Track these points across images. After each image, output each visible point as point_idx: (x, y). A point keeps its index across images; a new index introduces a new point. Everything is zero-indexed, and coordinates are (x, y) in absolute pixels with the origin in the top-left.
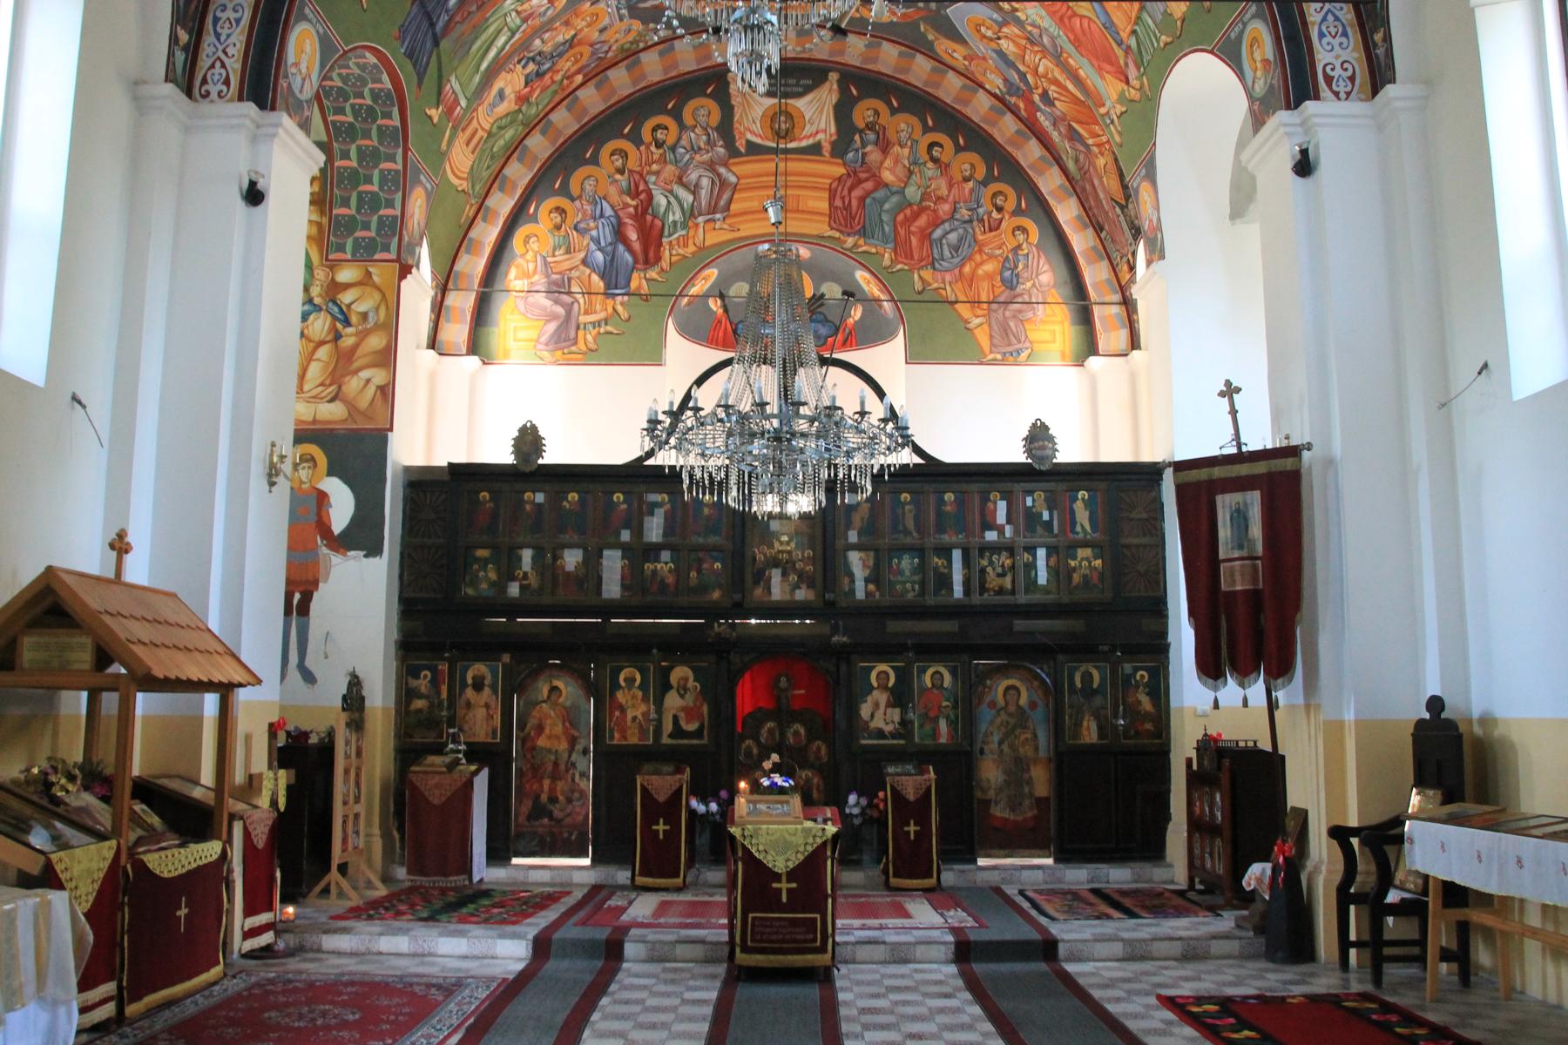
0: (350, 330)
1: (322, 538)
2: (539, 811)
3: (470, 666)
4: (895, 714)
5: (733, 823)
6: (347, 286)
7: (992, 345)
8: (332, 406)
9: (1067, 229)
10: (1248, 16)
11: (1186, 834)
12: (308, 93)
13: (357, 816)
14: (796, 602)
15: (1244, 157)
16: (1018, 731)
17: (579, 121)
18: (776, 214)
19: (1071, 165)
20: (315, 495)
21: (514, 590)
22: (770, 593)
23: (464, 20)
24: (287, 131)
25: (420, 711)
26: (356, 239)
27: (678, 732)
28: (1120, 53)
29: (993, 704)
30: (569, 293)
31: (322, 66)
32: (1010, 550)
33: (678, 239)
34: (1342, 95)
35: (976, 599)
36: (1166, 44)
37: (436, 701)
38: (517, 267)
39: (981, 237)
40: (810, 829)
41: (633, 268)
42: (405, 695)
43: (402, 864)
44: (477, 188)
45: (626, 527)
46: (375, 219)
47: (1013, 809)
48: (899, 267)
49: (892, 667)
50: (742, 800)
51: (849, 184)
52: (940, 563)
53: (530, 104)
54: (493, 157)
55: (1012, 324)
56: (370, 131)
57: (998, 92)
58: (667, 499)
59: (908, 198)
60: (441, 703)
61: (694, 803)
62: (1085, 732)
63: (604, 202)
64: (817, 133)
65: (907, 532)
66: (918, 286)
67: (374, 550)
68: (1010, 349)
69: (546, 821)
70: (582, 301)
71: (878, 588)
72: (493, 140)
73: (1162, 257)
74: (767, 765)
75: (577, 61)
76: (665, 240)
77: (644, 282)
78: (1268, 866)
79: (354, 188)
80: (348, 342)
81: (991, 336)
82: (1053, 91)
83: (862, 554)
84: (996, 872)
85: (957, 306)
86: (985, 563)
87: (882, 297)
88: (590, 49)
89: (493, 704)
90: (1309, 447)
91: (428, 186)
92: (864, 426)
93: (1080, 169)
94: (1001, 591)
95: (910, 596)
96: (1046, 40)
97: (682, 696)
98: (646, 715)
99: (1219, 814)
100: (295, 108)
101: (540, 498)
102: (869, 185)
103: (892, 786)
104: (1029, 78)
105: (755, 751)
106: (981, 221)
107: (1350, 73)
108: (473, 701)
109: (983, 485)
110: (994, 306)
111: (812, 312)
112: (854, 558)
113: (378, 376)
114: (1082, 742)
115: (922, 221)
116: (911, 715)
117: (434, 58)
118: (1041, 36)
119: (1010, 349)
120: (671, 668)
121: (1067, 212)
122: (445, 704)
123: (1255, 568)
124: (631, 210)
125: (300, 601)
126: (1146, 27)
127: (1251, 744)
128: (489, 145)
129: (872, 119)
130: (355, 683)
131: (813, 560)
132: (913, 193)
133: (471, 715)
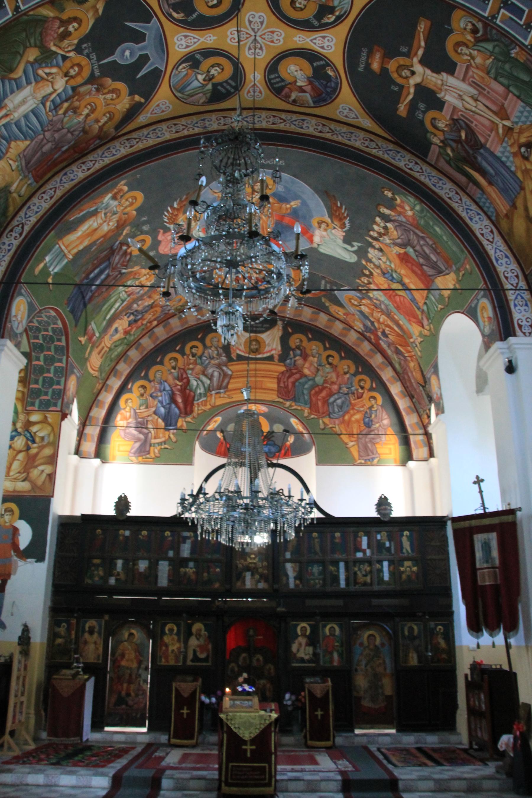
0: (35, 445)
1: (15, 552)
2: (121, 701)
4: (310, 650)
5: (221, 712)
8: (23, 484)
9: (396, 398)
12: (20, 329)
13: (22, 703)
17: (154, 343)
18: (247, 394)
19: (397, 366)
21: (112, 581)
23: (99, 295)
25: (59, 645)
27: (196, 658)
28: (419, 313)
29: (361, 644)
30: (147, 428)
31: (29, 317)
32: (369, 562)
33: (202, 402)
34: (527, 334)
35: (352, 588)
36: (441, 309)
38: (121, 414)
39: (353, 402)
41: (179, 416)
42: (52, 635)
43: (45, 730)
44: (103, 375)
46: (50, 391)
48: (312, 416)
49: (309, 625)
50: (227, 699)
51: (287, 375)
55: (369, 445)
57: (360, 330)
61: (203, 698)
62: (411, 659)
63: (166, 384)
64: (272, 350)
65: (316, 553)
66: (322, 426)
67: (40, 558)
68: (369, 458)
69: (124, 706)
70: (153, 432)
73: (443, 412)
74: (241, 679)
75: (154, 315)
76: (195, 402)
77: (184, 423)
79: (41, 375)
80: (33, 451)
81: (359, 451)
83: (293, 565)
84: (365, 738)
85: (342, 436)
86: (356, 569)
87: (304, 432)
89: (98, 642)
90: (520, 509)
91: (78, 374)
93: (402, 368)
94: (365, 584)
95: (318, 586)
97: (198, 639)
98: (179, 649)
100: (14, 337)
101: (127, 533)
102: (297, 376)
104: (376, 324)
106: (353, 393)
108: (88, 640)
109: (355, 528)
110: (360, 436)
112: (289, 566)
113: (48, 469)
114: (409, 665)
115: (324, 394)
116: (318, 651)
117: (84, 313)
118: (380, 305)
119: (369, 458)
121: (396, 389)
122: (74, 641)
124: (179, 387)
126: (431, 300)
127: (498, 667)
129: (298, 344)
130: (26, 629)
132: (319, 380)
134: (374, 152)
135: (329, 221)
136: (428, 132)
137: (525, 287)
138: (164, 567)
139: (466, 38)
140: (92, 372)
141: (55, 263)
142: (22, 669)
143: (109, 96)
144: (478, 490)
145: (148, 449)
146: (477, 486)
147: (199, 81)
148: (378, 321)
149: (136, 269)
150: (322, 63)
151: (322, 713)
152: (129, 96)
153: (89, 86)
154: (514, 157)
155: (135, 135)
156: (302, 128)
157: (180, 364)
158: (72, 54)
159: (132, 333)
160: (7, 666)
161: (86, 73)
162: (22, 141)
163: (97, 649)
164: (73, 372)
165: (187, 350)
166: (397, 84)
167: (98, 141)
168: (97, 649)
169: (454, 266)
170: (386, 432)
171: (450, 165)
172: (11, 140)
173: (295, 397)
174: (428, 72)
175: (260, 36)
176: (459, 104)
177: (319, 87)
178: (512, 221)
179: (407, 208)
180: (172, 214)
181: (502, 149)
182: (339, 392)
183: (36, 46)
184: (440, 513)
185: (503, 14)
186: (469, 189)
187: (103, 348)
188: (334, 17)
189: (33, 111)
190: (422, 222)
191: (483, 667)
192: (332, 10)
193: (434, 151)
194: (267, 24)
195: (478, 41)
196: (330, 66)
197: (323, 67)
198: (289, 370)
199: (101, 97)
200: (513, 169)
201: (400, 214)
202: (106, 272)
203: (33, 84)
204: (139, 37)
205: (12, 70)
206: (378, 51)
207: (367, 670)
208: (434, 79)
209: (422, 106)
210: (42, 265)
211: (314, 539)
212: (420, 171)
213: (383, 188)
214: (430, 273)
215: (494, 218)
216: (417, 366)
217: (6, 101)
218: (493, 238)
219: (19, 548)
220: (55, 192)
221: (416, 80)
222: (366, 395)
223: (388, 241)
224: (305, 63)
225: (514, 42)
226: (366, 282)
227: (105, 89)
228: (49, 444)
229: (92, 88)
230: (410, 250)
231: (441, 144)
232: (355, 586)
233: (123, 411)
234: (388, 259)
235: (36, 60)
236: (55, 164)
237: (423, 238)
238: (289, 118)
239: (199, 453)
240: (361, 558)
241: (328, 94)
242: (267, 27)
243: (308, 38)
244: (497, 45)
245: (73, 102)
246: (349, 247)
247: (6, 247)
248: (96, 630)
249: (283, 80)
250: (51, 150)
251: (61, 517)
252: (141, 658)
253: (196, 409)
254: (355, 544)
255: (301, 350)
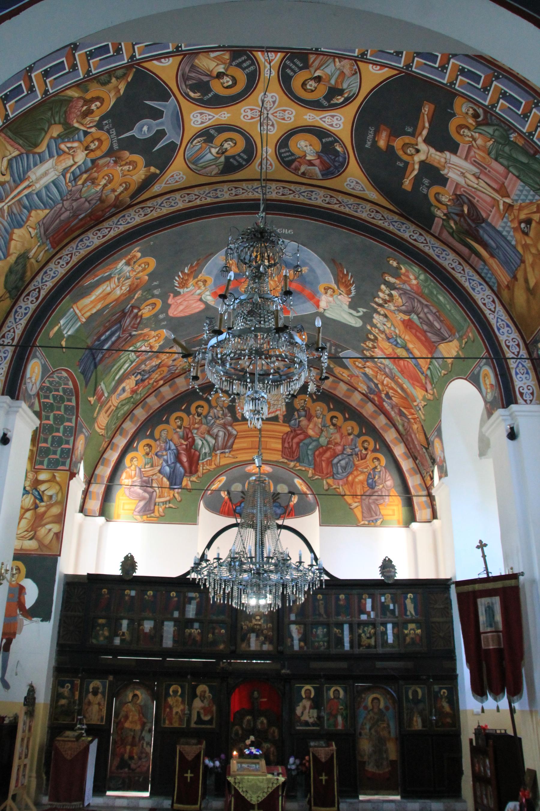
0: (43, 504)
1: (20, 611)
2: (123, 764)
3: (91, 682)
4: (314, 713)
5: (229, 775)
6: (43, 482)
7: (363, 517)
8: (31, 542)
9: (400, 459)
10: (482, 364)
11: (471, 783)
12: (34, 392)
13: (25, 766)
14: (264, 651)
15: (484, 429)
16: (380, 722)
17: (160, 403)
18: (258, 461)
19: (400, 428)
20: (18, 586)
21: (117, 641)
22: (249, 646)
23: (110, 356)
24: (23, 410)
25: (63, 706)
26: (49, 459)
27: (200, 721)
28: (423, 377)
29: (366, 708)
30: (152, 487)
31: (42, 379)
32: (373, 624)
34: (528, 402)
35: (357, 651)
36: (445, 375)
37: (72, 700)
38: (127, 473)
39: (357, 463)
40: (270, 779)
41: (184, 475)
42: (56, 696)
43: (46, 794)
44: (109, 433)
45: (177, 610)
46: (59, 449)
47: (378, 767)
48: (316, 477)
49: (313, 687)
50: (235, 762)
51: (292, 435)
52: (337, 631)
53: (137, 394)
54: (117, 419)
55: (373, 506)
56: (60, 407)
57: (364, 392)
58: (198, 596)
59: (321, 442)
60: (74, 702)
61: (207, 761)
62: (415, 724)
63: (171, 443)
64: (276, 411)
65: (320, 615)
66: (326, 487)
67: (46, 618)
68: (372, 519)
69: (126, 770)
70: (158, 491)
71: (306, 644)
72: (118, 410)
73: (446, 475)
74: (248, 742)
75: (161, 374)
76: (200, 462)
77: (189, 482)
78: (517, 803)
79: (50, 434)
80: (41, 510)
81: (362, 512)
82: (391, 393)
83: (298, 626)
84: (370, 804)
85: (345, 497)
86: (361, 631)
87: (308, 492)
88: (167, 369)
89: (102, 703)
90: (522, 574)
91: (86, 434)
92: (301, 568)
93: (405, 430)
94: (369, 646)
95: (322, 648)
96: (387, 370)
97: (202, 701)
98: (183, 710)
99: (489, 772)
100: (27, 398)
101: (133, 593)
102: (302, 437)
103: (313, 754)
104: (380, 386)
105: (240, 732)
106: (357, 455)
107: (531, 391)
108: (92, 701)
109: (359, 590)
110: (364, 497)
111: (274, 501)
112: (294, 628)
113: (55, 528)
114: (413, 729)
115: (328, 454)
116: (323, 713)
117: (94, 374)
119: (372, 519)
120: (197, 686)
121: (399, 451)
122: (77, 702)
123: (499, 637)
124: (184, 446)
125: (5, 644)
126: (434, 366)
127: (503, 732)
128: (116, 413)
130: (32, 690)
131: (272, 629)
132: (323, 441)
133: (90, 709)
134: (380, 223)
135: (335, 287)
136: (432, 205)
137: (526, 356)
138: (169, 628)
139: (467, 122)
140: (99, 430)
141: (68, 327)
142: (27, 731)
143: (126, 168)
144: (481, 554)
145: (152, 507)
146: (480, 550)
147: (212, 154)
148: (382, 383)
149: (146, 331)
150: (330, 139)
151: (326, 778)
152: (145, 167)
153: (108, 159)
154: (514, 232)
155: (149, 204)
156: (310, 199)
157: (186, 424)
158: (93, 130)
159: (139, 392)
160: (13, 727)
161: (105, 147)
162: (42, 210)
163: (100, 710)
164: (82, 432)
165: (193, 409)
166: (401, 160)
167: (113, 210)
168: (100, 710)
169: (457, 334)
170: (389, 493)
171: (453, 237)
172: (32, 209)
173: (299, 457)
174: (432, 150)
175: (272, 114)
176: (461, 181)
177: (328, 161)
178: (513, 291)
179: (412, 277)
180: (183, 279)
181: (503, 225)
182: (343, 453)
183: (60, 123)
184: (443, 576)
185: (502, 103)
186: (471, 259)
187: (110, 406)
188: (343, 99)
189: (54, 182)
190: (426, 291)
191: (487, 732)
192: (341, 92)
193: (438, 223)
194: (279, 102)
195: (479, 124)
196: (338, 142)
197: (332, 143)
198: (293, 431)
199: (119, 169)
200: (513, 243)
201: (405, 282)
202: (117, 334)
203: (56, 157)
204: (157, 114)
205: (36, 145)
206: (385, 130)
207: (371, 734)
208: (437, 157)
209: (426, 181)
210: (56, 328)
211: (318, 600)
212: (425, 242)
213: (389, 257)
214: (433, 340)
215: (495, 289)
216: (420, 428)
217: (29, 173)
218: (495, 308)
219: (25, 607)
220: (71, 257)
221: (421, 157)
222: (370, 456)
223: (393, 308)
224: (315, 140)
225: (515, 130)
226: (370, 346)
227: (122, 161)
228: (57, 503)
229: (111, 160)
230: (414, 317)
231: (445, 217)
232: (359, 648)
233: (128, 470)
234: (392, 324)
235: (59, 136)
236: (72, 231)
237: (427, 306)
238: (298, 189)
239: (204, 513)
240: (366, 620)
241: (336, 168)
242: (279, 106)
243: (318, 116)
244: (497, 130)
245: (91, 173)
246: (354, 313)
247: (23, 311)
248: (100, 691)
249: (293, 154)
250: (69, 218)
251: (66, 576)
252: (145, 720)
253: (201, 468)
254: (359, 606)
255: (306, 411)
